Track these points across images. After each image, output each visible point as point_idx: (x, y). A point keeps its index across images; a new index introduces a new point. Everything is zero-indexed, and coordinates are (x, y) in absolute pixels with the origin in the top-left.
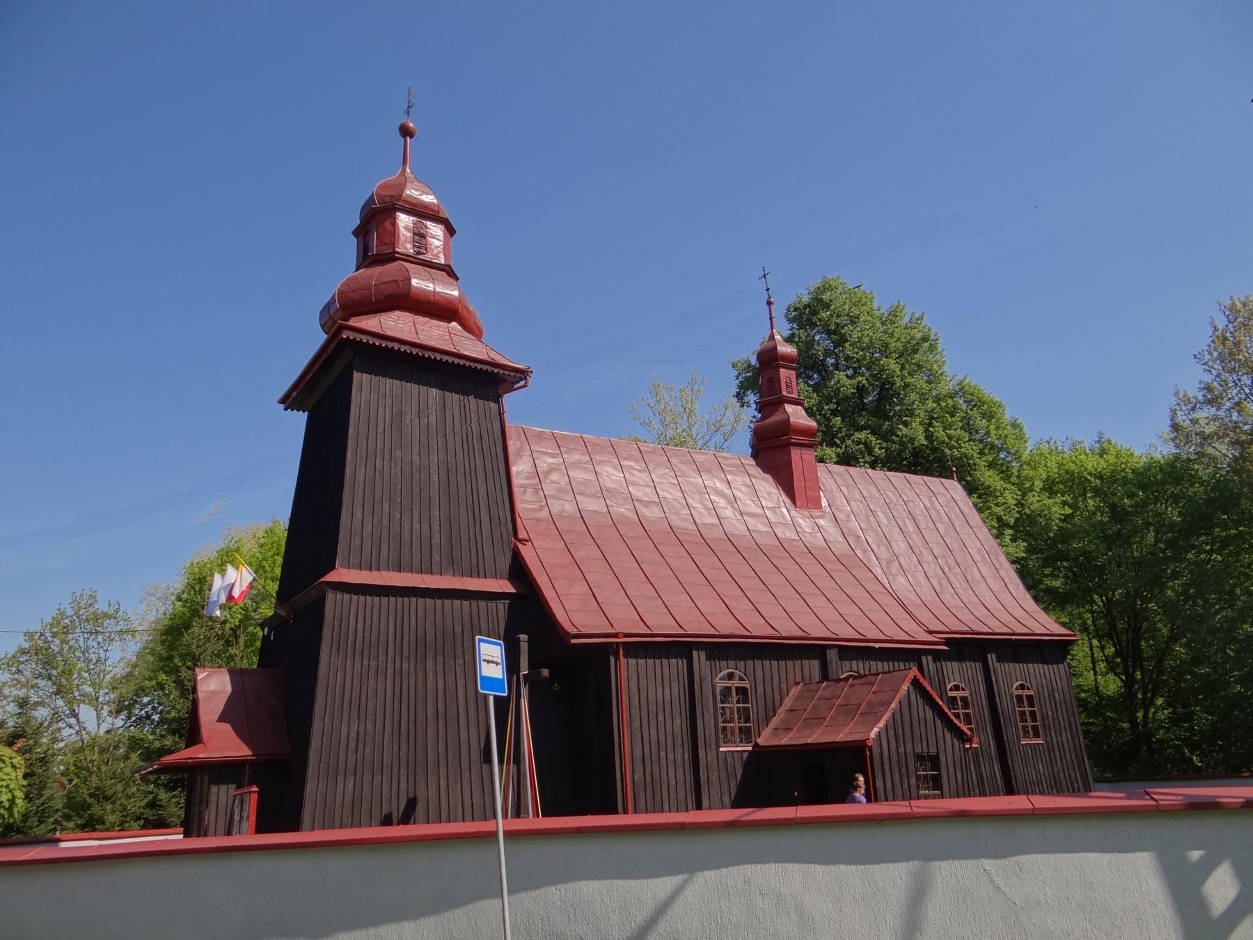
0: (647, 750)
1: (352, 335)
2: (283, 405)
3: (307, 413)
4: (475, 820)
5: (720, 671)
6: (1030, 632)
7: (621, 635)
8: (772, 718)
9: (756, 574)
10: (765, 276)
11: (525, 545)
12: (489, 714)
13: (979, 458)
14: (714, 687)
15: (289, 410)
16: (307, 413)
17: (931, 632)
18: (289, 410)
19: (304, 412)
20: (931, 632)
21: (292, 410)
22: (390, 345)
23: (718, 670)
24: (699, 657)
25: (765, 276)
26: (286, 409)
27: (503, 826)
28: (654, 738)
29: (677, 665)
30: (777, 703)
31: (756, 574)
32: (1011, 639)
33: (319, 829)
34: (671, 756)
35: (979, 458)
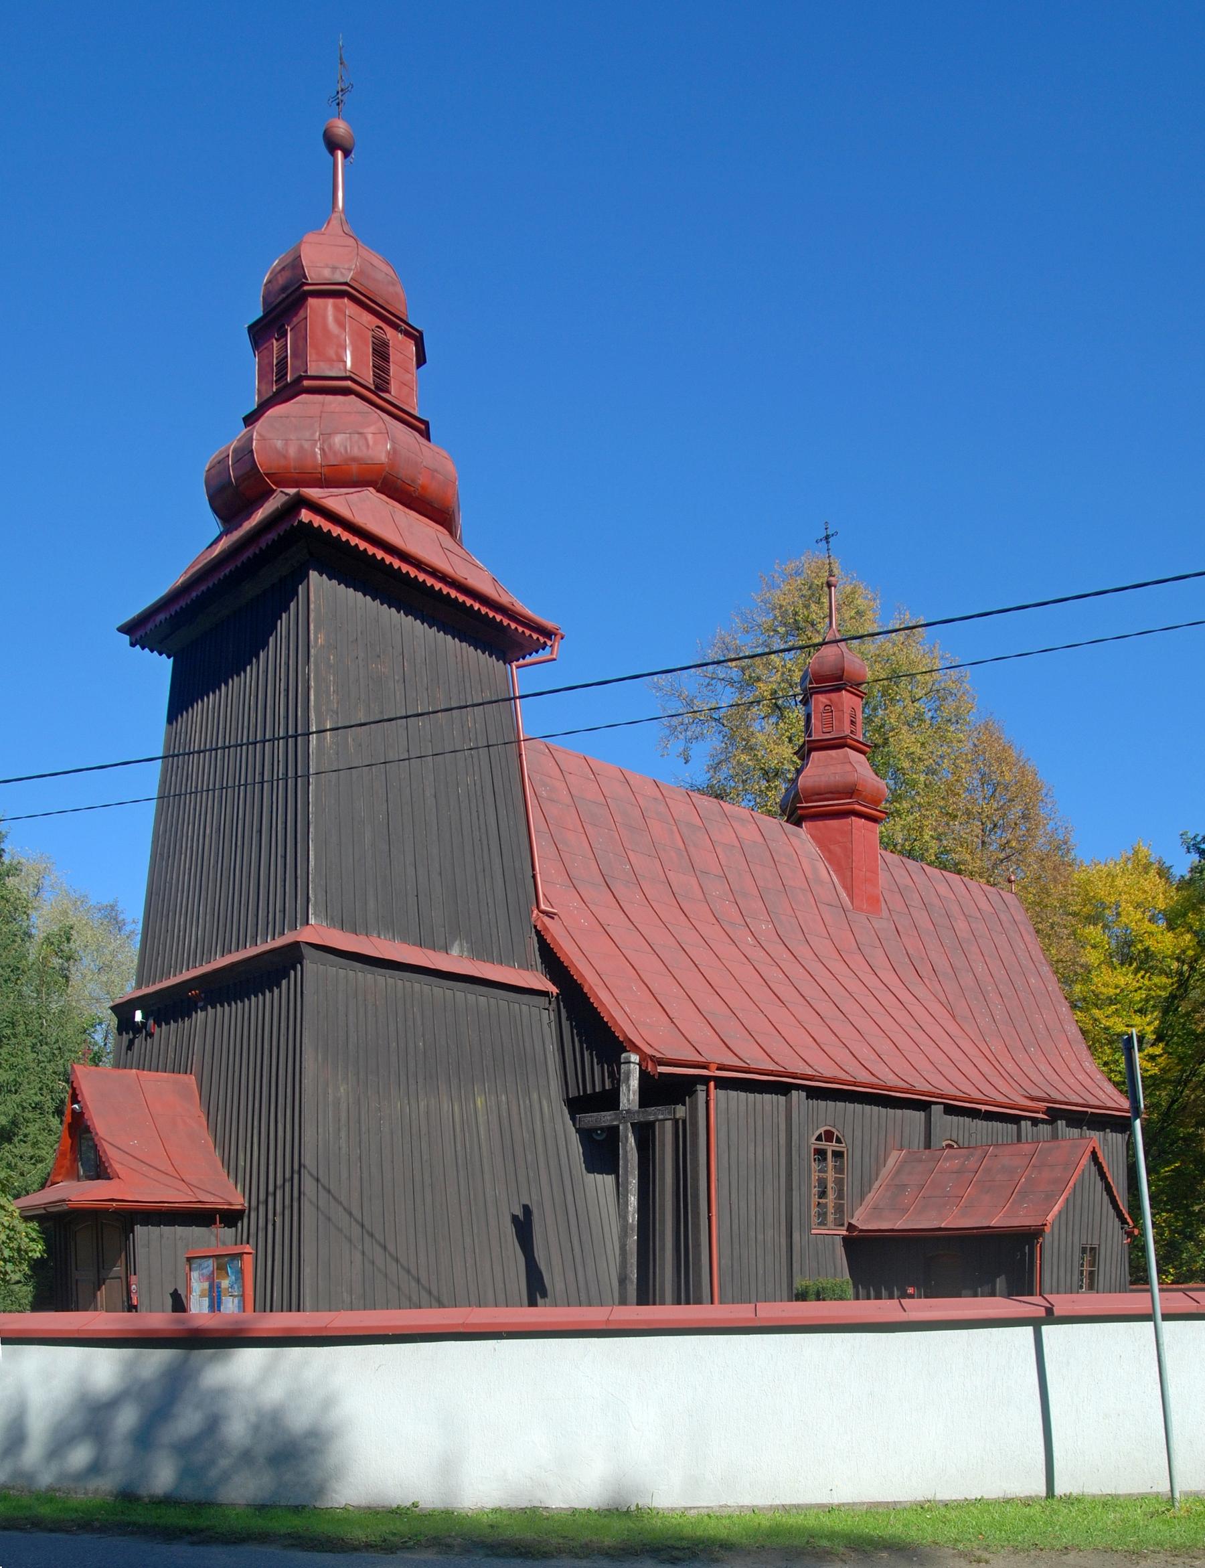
0: (735, 1227)
1: (318, 521)
2: (127, 637)
3: (172, 658)
4: (274, 1309)
5: (818, 1128)
6: (1085, 1102)
7: (713, 1067)
8: (867, 1194)
9: (829, 997)
10: (827, 538)
11: (553, 918)
12: (698, 1165)
13: (947, 852)
14: (809, 1147)
15: (138, 646)
16: (172, 658)
17: (1032, 1099)
18: (138, 646)
19: (169, 657)
20: (1032, 1099)
21: (143, 648)
22: (372, 550)
23: (815, 1128)
24: (937, 1110)
25: (827, 538)
26: (133, 645)
27: (1161, 1304)
28: (743, 1211)
29: (920, 1116)
30: (873, 1177)
31: (829, 997)
32: (1087, 1112)
33: (287, 1311)
34: (760, 1237)
35: (947, 852)
